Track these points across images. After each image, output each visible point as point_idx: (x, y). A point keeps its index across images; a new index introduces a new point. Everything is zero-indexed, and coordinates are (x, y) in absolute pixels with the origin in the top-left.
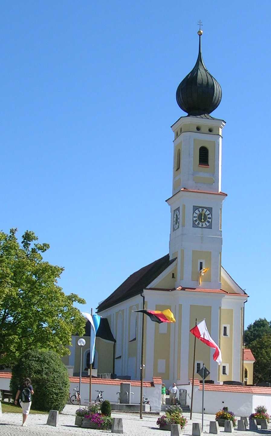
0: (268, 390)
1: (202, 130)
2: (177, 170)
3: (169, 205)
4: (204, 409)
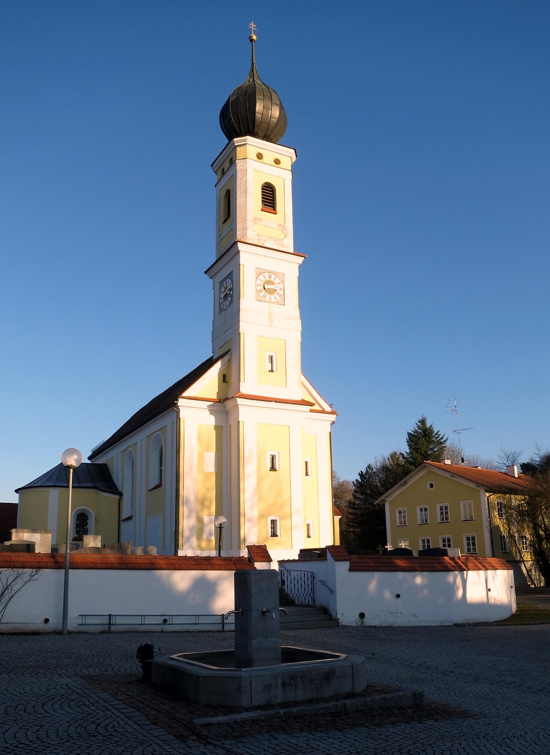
0: (338, 543)
1: (265, 159)
2: (224, 222)
3: (210, 278)
4: (489, 590)
